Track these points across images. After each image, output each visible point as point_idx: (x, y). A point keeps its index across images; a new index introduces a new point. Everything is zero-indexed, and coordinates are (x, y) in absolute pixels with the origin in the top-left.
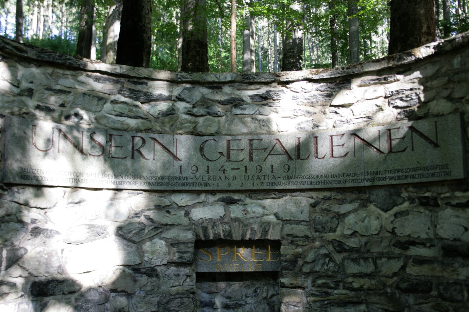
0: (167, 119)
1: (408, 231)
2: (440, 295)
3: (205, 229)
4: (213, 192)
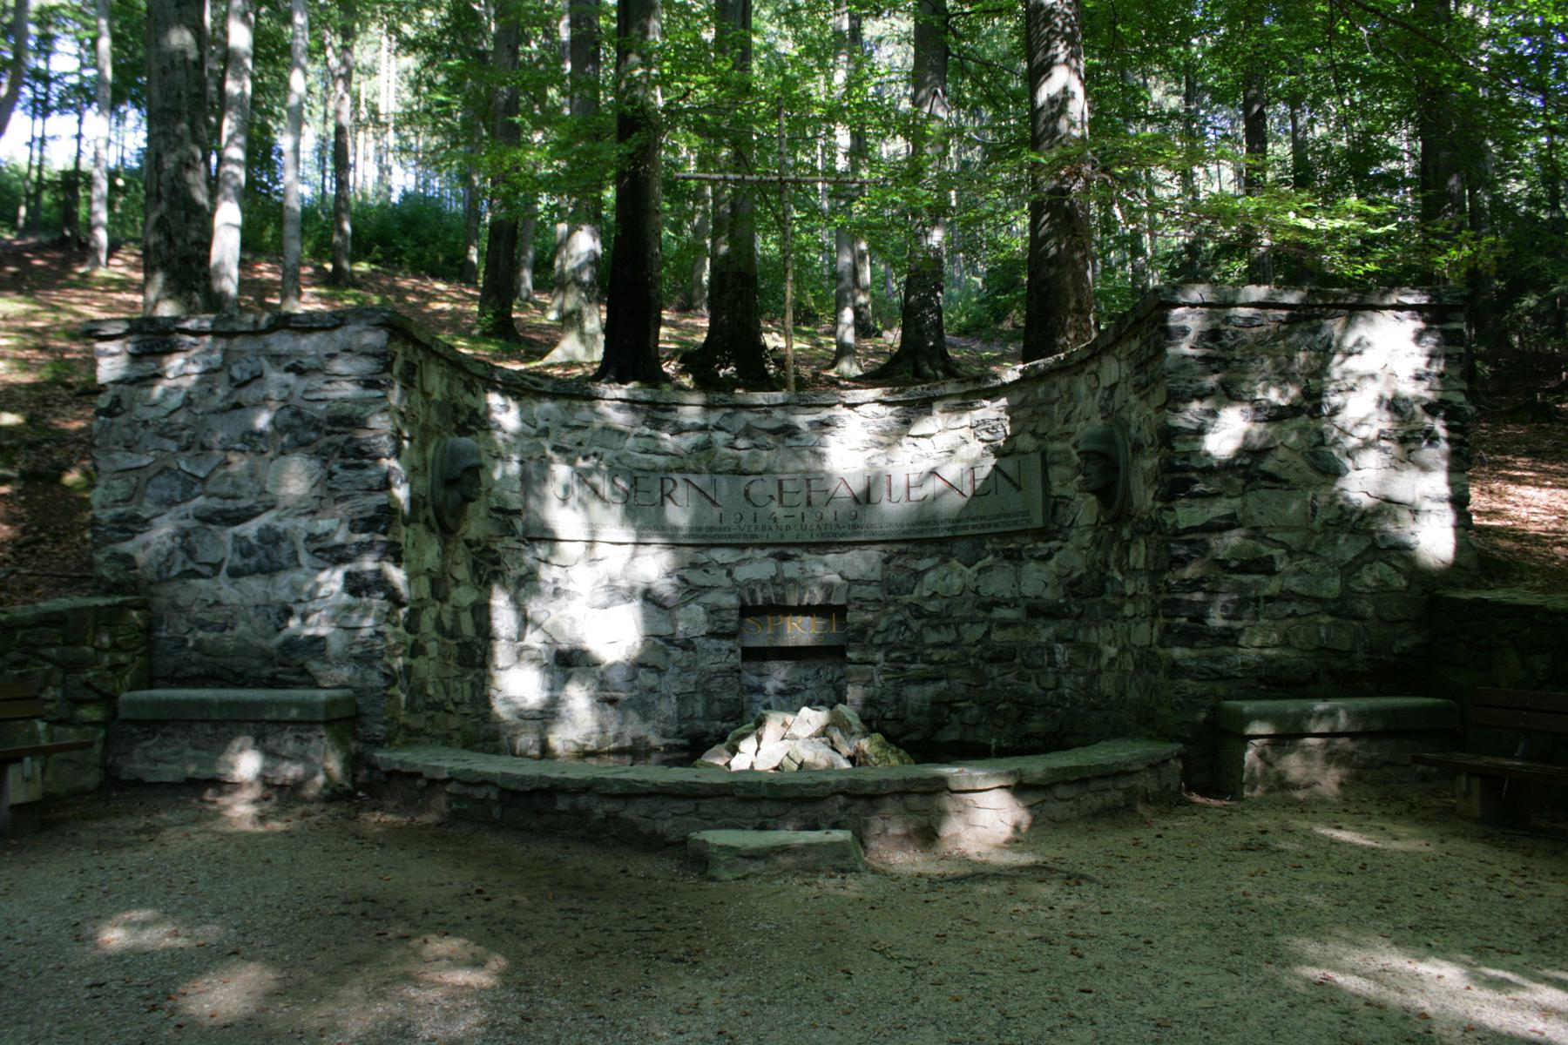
0: (702, 455)
1: (991, 590)
2: (1024, 663)
3: (752, 593)
4: (762, 546)
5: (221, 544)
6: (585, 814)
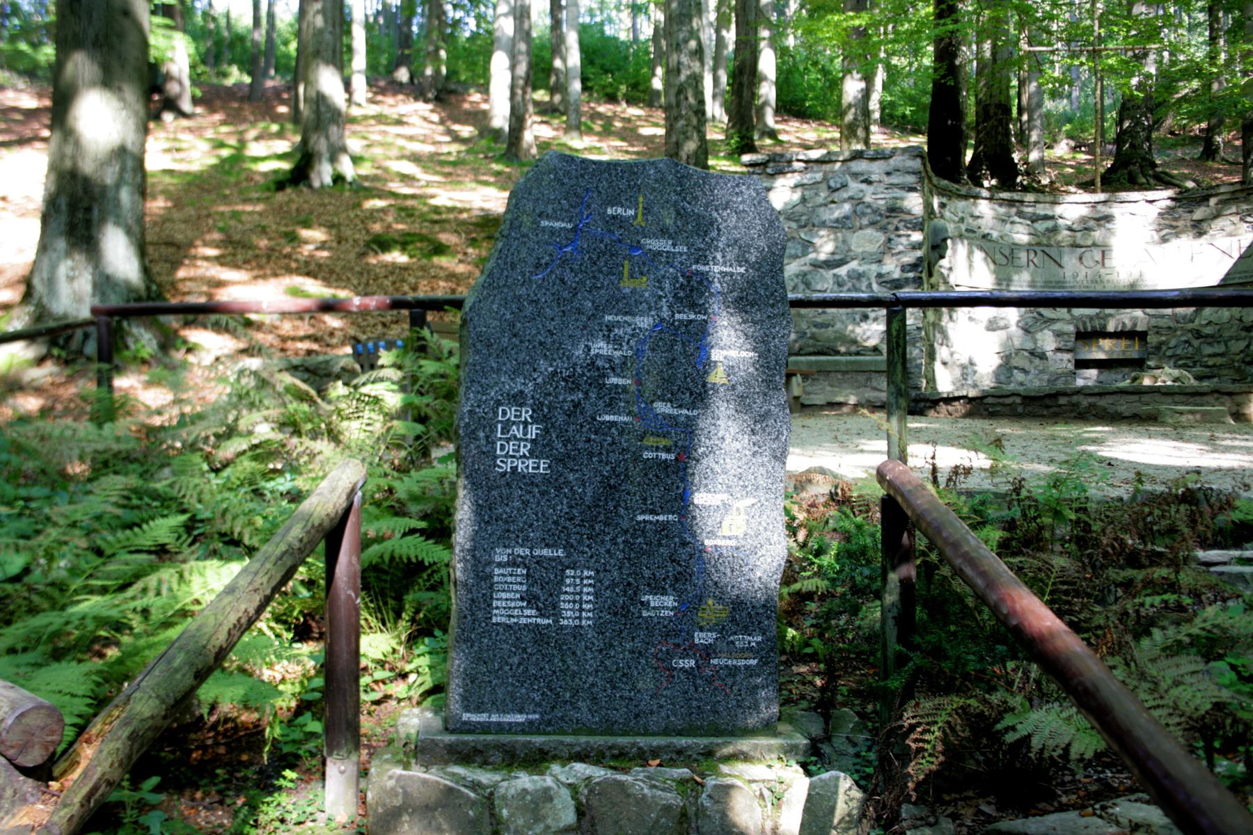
3: (1084, 324)
5: (823, 279)
6: (1076, 405)
